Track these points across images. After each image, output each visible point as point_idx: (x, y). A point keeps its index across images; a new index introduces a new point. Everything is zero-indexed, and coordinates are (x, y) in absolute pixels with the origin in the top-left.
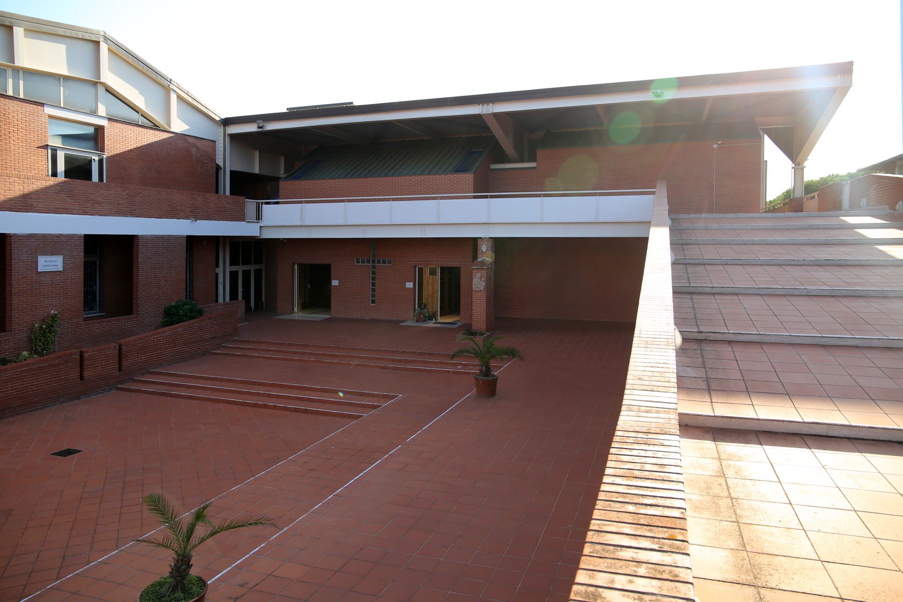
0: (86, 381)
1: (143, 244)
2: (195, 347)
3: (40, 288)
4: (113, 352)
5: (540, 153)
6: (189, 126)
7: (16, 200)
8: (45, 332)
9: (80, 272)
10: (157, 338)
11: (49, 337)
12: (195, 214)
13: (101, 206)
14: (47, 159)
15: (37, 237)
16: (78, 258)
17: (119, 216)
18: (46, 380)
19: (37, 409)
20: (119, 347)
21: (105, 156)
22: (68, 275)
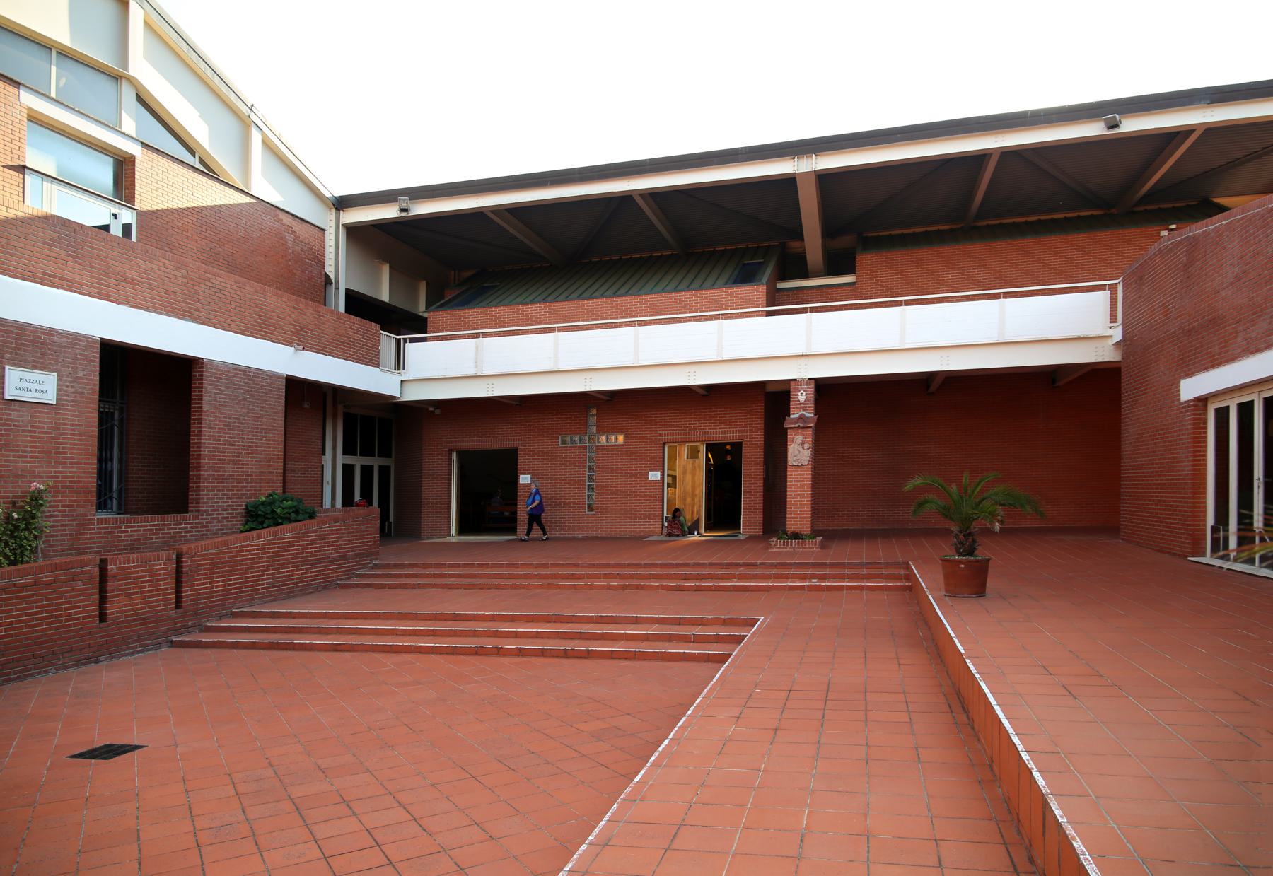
0: (112, 624)
1: (212, 377)
2: (311, 572)
3: (8, 435)
4: (164, 565)
5: (862, 261)
8: (17, 528)
9: (89, 412)
10: (247, 546)
11: (26, 538)
14: (21, 195)
16: (88, 384)
18: (27, 615)
20: (177, 558)
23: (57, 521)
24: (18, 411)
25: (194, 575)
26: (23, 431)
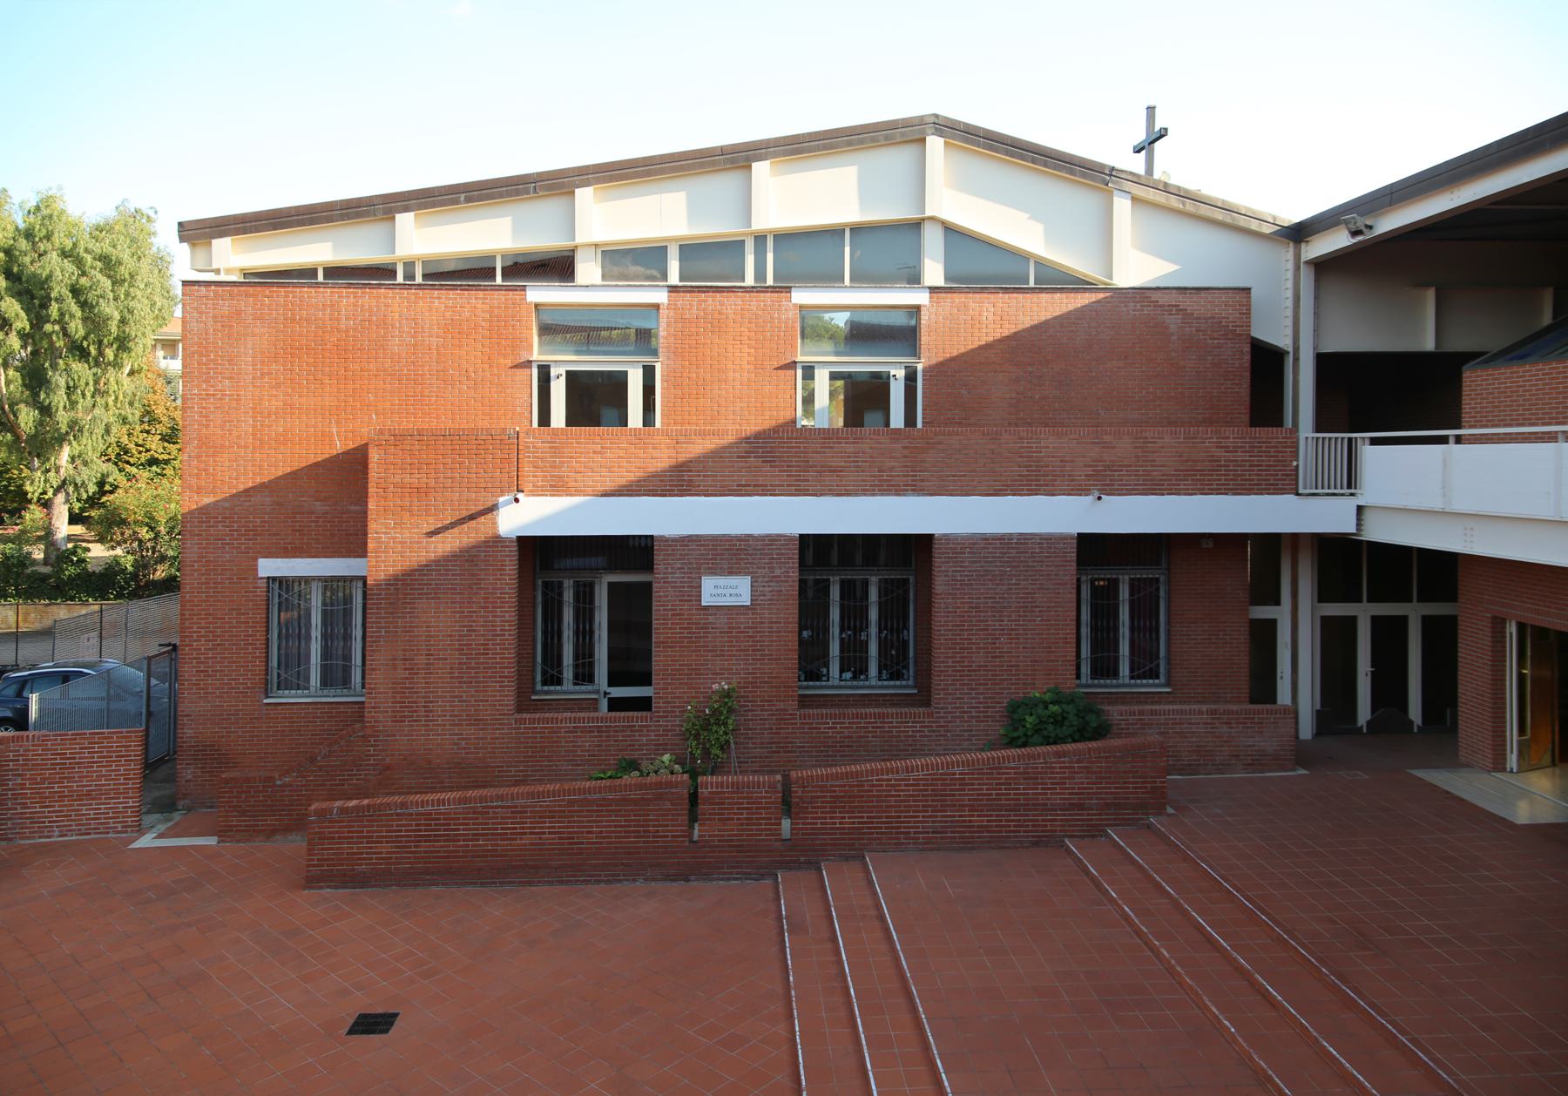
6: (1175, 263)
7: (662, 476)
12: (1105, 481)
13: (837, 476)
15: (700, 541)
17: (882, 495)
19: (599, 882)
21: (920, 367)
22: (764, 614)
23: (756, 715)
24: (715, 614)
25: (807, 808)
26: (720, 632)
